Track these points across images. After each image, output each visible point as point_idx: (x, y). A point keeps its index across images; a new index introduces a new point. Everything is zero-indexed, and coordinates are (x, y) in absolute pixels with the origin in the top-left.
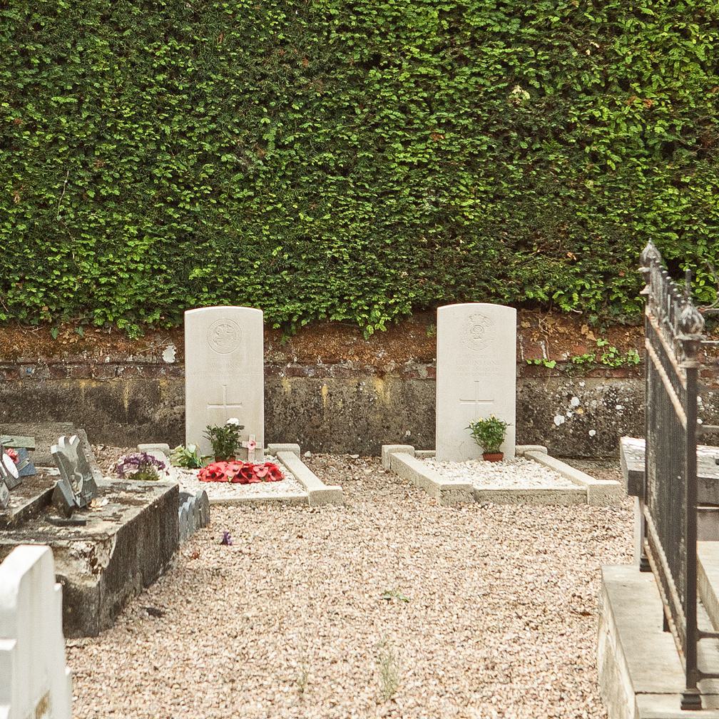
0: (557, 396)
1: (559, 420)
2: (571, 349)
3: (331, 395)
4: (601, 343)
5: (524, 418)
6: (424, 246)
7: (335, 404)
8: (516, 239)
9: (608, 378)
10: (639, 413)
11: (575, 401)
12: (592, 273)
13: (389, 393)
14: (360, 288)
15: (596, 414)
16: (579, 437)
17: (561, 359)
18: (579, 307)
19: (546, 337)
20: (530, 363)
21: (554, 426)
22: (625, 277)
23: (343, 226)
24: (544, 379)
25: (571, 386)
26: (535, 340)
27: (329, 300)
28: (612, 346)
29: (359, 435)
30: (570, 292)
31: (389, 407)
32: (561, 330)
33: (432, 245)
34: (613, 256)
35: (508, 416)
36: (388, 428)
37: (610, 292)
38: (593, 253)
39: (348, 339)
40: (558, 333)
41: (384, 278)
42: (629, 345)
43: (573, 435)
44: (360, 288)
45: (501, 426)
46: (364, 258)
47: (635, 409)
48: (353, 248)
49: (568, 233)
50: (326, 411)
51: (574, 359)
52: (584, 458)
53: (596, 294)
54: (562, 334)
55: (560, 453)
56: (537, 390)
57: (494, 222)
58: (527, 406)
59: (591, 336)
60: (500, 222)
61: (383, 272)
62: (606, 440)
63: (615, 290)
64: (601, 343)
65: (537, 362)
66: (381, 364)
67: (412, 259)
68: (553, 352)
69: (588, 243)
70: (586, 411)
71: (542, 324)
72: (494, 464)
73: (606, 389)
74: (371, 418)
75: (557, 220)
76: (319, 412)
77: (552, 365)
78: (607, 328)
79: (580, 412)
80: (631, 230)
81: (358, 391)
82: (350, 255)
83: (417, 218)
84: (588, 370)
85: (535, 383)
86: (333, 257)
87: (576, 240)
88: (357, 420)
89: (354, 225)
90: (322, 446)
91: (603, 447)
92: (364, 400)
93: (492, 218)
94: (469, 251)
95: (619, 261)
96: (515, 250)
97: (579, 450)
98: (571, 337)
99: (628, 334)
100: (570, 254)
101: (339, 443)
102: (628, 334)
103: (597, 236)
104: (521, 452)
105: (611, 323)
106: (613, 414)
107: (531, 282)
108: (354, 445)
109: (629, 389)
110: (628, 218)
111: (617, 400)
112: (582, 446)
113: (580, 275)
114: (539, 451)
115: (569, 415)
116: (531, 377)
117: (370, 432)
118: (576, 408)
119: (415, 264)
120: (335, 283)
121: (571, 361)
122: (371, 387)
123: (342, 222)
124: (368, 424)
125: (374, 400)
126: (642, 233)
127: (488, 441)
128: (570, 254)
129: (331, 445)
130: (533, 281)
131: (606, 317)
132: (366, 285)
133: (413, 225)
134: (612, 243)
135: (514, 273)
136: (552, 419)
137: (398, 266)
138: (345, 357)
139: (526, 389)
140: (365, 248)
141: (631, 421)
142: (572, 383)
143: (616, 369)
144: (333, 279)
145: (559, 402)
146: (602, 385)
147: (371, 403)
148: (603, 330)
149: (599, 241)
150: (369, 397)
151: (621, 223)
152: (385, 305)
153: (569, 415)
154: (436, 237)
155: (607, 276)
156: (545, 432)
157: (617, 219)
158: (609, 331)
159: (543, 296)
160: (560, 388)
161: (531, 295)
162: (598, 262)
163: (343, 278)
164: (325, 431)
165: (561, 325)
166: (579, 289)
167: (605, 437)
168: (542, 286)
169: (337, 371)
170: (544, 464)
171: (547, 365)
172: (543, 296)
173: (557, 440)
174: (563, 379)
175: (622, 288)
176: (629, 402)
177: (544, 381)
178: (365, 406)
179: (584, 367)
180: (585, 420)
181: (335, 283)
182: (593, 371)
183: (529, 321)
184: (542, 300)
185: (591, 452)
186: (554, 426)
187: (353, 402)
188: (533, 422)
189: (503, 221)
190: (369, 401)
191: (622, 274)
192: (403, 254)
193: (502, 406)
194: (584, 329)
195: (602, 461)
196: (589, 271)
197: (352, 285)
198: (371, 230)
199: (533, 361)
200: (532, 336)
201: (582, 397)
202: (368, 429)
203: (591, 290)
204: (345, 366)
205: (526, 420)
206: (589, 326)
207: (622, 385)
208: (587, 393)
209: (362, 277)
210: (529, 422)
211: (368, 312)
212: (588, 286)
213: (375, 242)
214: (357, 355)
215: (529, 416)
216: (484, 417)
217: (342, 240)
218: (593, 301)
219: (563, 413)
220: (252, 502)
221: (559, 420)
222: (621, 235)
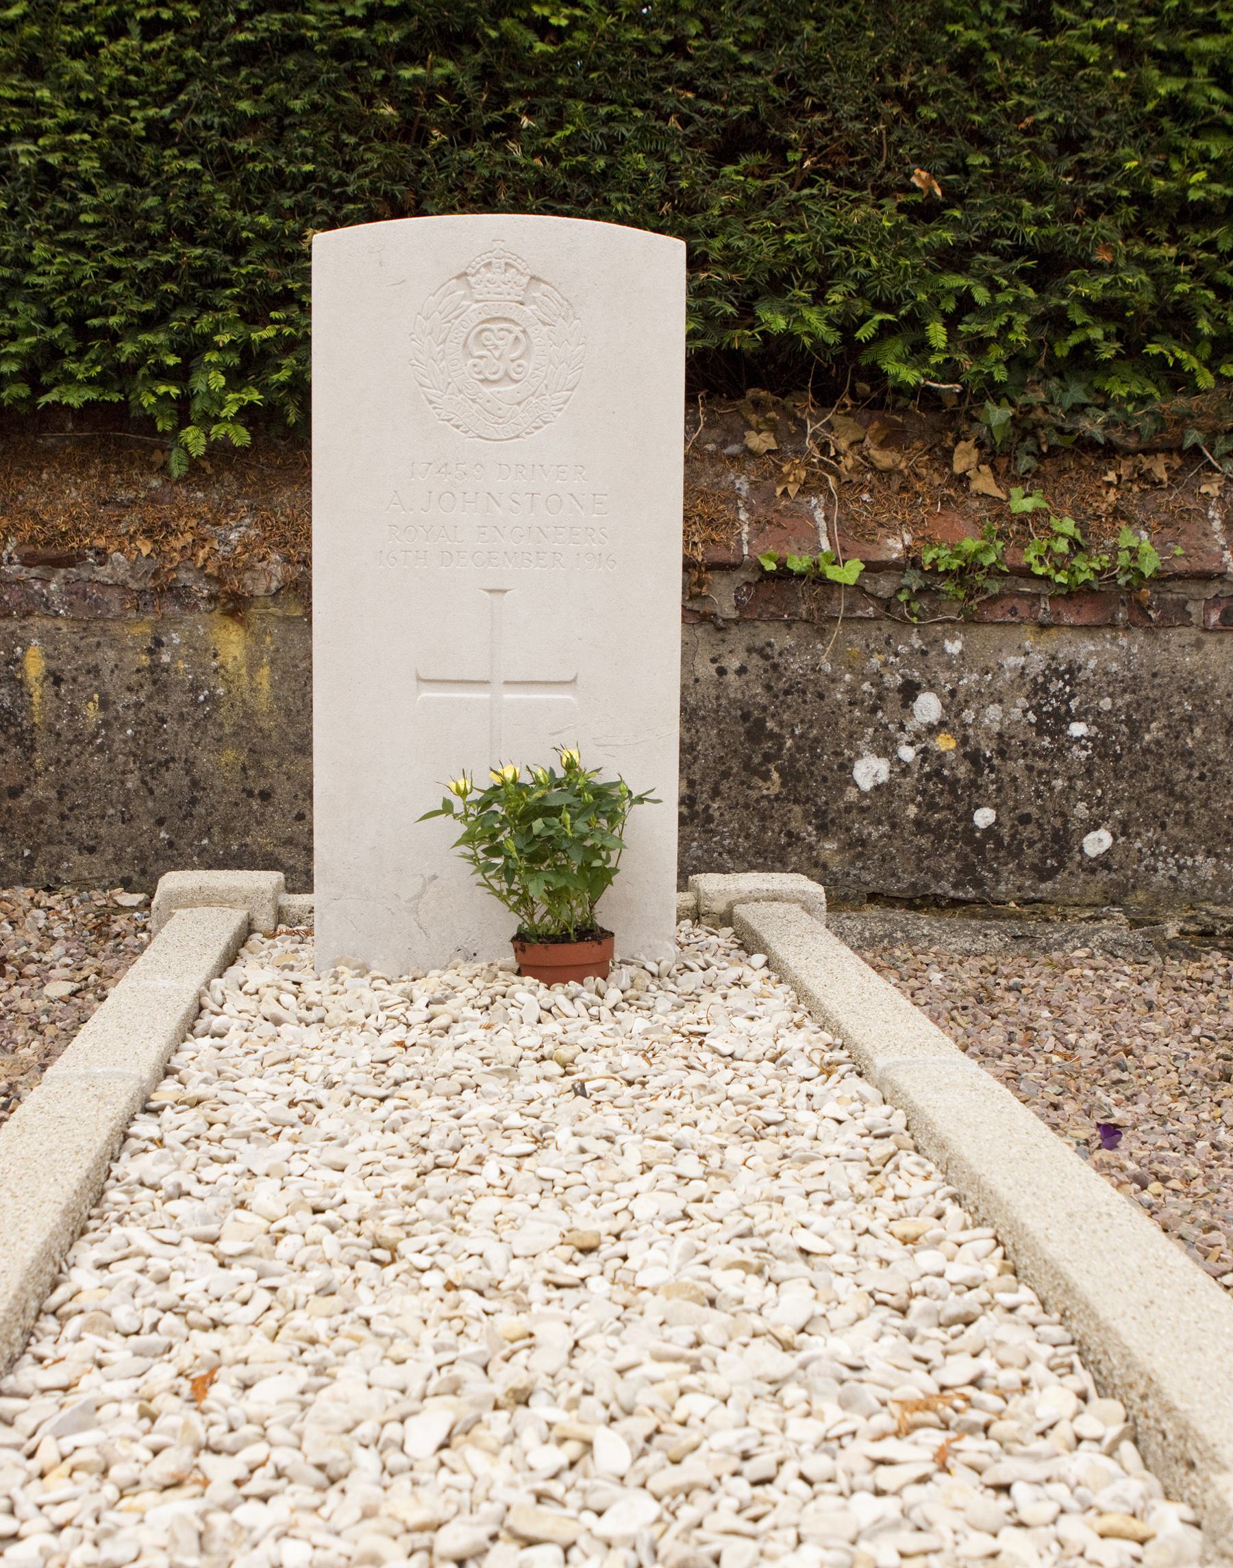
0: (866, 686)
1: (870, 771)
2: (915, 525)
3: (58, 681)
4: (1022, 504)
5: (747, 766)
6: (386, 134)
7: (74, 712)
8: (724, 116)
9: (1043, 627)
10: (1146, 751)
11: (928, 707)
12: (995, 252)
13: (266, 671)
14: (144, 284)
15: (1001, 753)
16: (937, 832)
17: (883, 557)
18: (950, 371)
19: (832, 481)
20: (771, 566)
21: (851, 795)
22: (1113, 268)
23: (75, 51)
24: (819, 626)
25: (913, 652)
26: (793, 490)
27: (30, 331)
28: (1060, 516)
29: (160, 822)
30: (915, 322)
31: (267, 724)
32: (885, 459)
33: (412, 131)
34: (1075, 194)
35: (644, 757)
36: (265, 796)
37: (1058, 322)
38: (1001, 178)
39: (129, 484)
40: (873, 469)
41: (237, 249)
42: (1117, 513)
43: (918, 823)
44: (144, 284)
45: (605, 803)
46: (158, 172)
47: (1135, 735)
48: (118, 134)
49: (910, 102)
50: (42, 738)
51: (928, 557)
52: (956, 903)
53: (1008, 327)
54: (885, 474)
55: (873, 888)
56: (796, 665)
57: (642, 49)
58: (760, 723)
59: (984, 482)
60: (667, 48)
61: (228, 224)
62: (1031, 844)
63: (1078, 316)
64: (1022, 504)
65: (797, 564)
66: (229, 567)
67: (342, 183)
68: (854, 532)
69: (980, 139)
70: (964, 741)
71: (815, 435)
72: (558, 995)
73: (1037, 664)
74: (205, 760)
75: (874, 48)
76: (19, 739)
77: (849, 573)
78: (1040, 457)
79: (945, 743)
80: (1140, 96)
81: (155, 667)
82: (104, 158)
83: (352, 21)
84: (974, 594)
85: (789, 641)
86: (44, 166)
87: (939, 128)
88: (154, 768)
89: (118, 47)
90: (30, 861)
91: (1020, 867)
92: (177, 697)
93: (636, 34)
94: (553, 157)
95: (1093, 211)
96: (724, 154)
97: (938, 876)
98: (918, 486)
99: (1111, 477)
100: (919, 177)
101: (92, 850)
102: (1111, 477)
103: (1019, 112)
104: (719, 906)
105: (1055, 439)
106: (1059, 753)
107: (777, 285)
108: (143, 858)
109: (1114, 667)
110: (1127, 49)
111: (1073, 704)
112: (948, 863)
113: (952, 259)
114: (786, 902)
115: (907, 753)
116: (775, 618)
117: (200, 810)
118: (932, 730)
119: (353, 199)
120: (50, 265)
121: (915, 563)
122: (201, 651)
123: (69, 34)
124: (195, 784)
125: (212, 699)
126: (1176, 107)
127: (546, 870)
128: (919, 177)
129: (61, 858)
130: (787, 278)
131: (1039, 414)
132: (169, 272)
133: (343, 50)
134: (1068, 142)
135: (717, 243)
136: (846, 767)
137: (287, 203)
138: (101, 542)
139: (756, 659)
140: (159, 133)
141: (1118, 776)
142: (917, 643)
143: (1075, 594)
144: (40, 250)
145: (874, 710)
146: (1023, 653)
147: (203, 707)
148: (1026, 462)
149: (1026, 133)
150: (195, 688)
151: (1109, 68)
152: (243, 348)
153: (907, 753)
154: (432, 103)
155: (1048, 266)
156: (821, 814)
157: (1093, 52)
158: (1048, 467)
159: (822, 328)
160: (876, 661)
161: (779, 323)
162: (1018, 210)
163: (78, 246)
164: (39, 807)
165: (883, 445)
166: (950, 306)
167: (1029, 831)
168: (819, 298)
169: (75, 591)
170: (807, 1004)
171: (833, 573)
172: (822, 328)
173: (863, 842)
174: (887, 628)
175: (1100, 310)
176: (1113, 712)
177: (821, 633)
178: (182, 718)
179: (961, 585)
180: (962, 771)
181: (50, 265)
182: (994, 599)
183: (774, 428)
184: (820, 345)
185: (978, 883)
186: (851, 795)
187: (139, 705)
188: (754, 782)
189: (678, 46)
190: (195, 703)
191: (1104, 257)
192: (306, 159)
193: (616, 697)
194: (964, 458)
195: (1019, 917)
196: (984, 244)
197: (115, 274)
198: (181, 63)
199: (781, 563)
200: (782, 479)
201: (953, 693)
202: (194, 801)
203: (991, 311)
204: (103, 573)
205: (755, 772)
206: (980, 445)
207: (1091, 652)
208: (969, 680)
209: (155, 242)
210: (766, 777)
211: (181, 375)
212: (981, 295)
213: (198, 110)
214: (149, 533)
215: (767, 758)
216: (527, 759)
217: (79, 104)
218: (996, 352)
219: (886, 748)
220: (135, 954)
221: (870, 771)
222: (1101, 111)
